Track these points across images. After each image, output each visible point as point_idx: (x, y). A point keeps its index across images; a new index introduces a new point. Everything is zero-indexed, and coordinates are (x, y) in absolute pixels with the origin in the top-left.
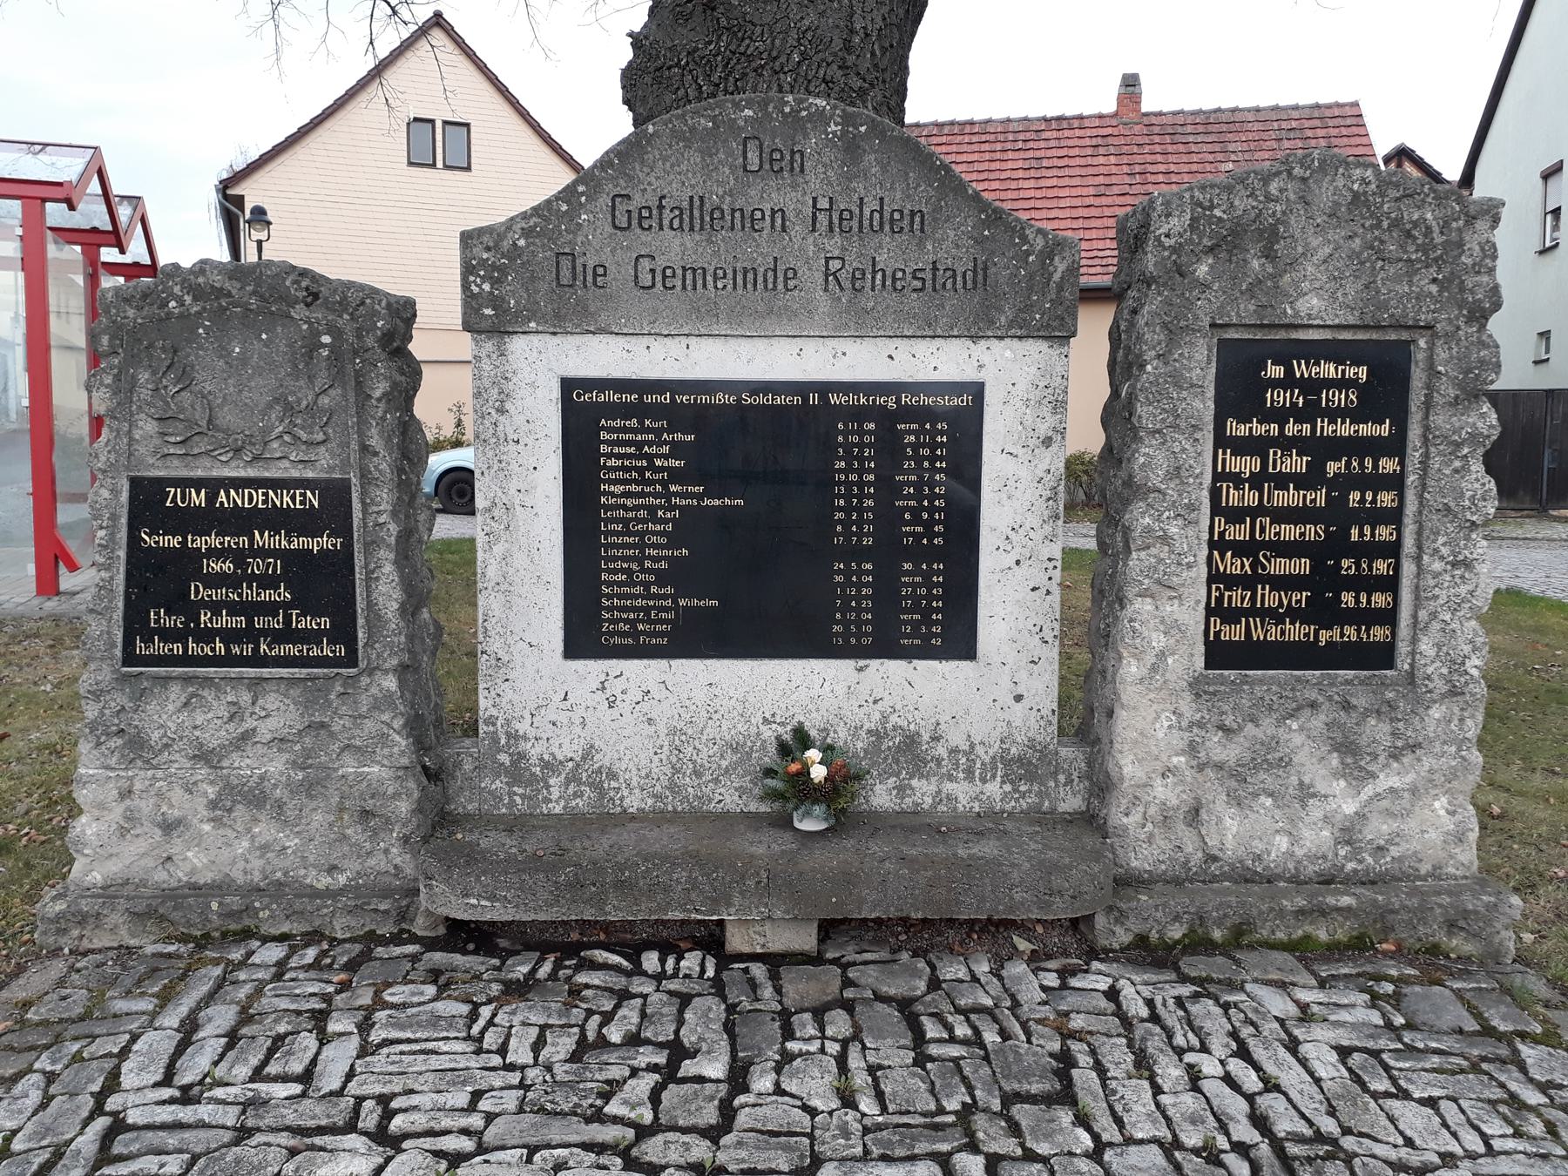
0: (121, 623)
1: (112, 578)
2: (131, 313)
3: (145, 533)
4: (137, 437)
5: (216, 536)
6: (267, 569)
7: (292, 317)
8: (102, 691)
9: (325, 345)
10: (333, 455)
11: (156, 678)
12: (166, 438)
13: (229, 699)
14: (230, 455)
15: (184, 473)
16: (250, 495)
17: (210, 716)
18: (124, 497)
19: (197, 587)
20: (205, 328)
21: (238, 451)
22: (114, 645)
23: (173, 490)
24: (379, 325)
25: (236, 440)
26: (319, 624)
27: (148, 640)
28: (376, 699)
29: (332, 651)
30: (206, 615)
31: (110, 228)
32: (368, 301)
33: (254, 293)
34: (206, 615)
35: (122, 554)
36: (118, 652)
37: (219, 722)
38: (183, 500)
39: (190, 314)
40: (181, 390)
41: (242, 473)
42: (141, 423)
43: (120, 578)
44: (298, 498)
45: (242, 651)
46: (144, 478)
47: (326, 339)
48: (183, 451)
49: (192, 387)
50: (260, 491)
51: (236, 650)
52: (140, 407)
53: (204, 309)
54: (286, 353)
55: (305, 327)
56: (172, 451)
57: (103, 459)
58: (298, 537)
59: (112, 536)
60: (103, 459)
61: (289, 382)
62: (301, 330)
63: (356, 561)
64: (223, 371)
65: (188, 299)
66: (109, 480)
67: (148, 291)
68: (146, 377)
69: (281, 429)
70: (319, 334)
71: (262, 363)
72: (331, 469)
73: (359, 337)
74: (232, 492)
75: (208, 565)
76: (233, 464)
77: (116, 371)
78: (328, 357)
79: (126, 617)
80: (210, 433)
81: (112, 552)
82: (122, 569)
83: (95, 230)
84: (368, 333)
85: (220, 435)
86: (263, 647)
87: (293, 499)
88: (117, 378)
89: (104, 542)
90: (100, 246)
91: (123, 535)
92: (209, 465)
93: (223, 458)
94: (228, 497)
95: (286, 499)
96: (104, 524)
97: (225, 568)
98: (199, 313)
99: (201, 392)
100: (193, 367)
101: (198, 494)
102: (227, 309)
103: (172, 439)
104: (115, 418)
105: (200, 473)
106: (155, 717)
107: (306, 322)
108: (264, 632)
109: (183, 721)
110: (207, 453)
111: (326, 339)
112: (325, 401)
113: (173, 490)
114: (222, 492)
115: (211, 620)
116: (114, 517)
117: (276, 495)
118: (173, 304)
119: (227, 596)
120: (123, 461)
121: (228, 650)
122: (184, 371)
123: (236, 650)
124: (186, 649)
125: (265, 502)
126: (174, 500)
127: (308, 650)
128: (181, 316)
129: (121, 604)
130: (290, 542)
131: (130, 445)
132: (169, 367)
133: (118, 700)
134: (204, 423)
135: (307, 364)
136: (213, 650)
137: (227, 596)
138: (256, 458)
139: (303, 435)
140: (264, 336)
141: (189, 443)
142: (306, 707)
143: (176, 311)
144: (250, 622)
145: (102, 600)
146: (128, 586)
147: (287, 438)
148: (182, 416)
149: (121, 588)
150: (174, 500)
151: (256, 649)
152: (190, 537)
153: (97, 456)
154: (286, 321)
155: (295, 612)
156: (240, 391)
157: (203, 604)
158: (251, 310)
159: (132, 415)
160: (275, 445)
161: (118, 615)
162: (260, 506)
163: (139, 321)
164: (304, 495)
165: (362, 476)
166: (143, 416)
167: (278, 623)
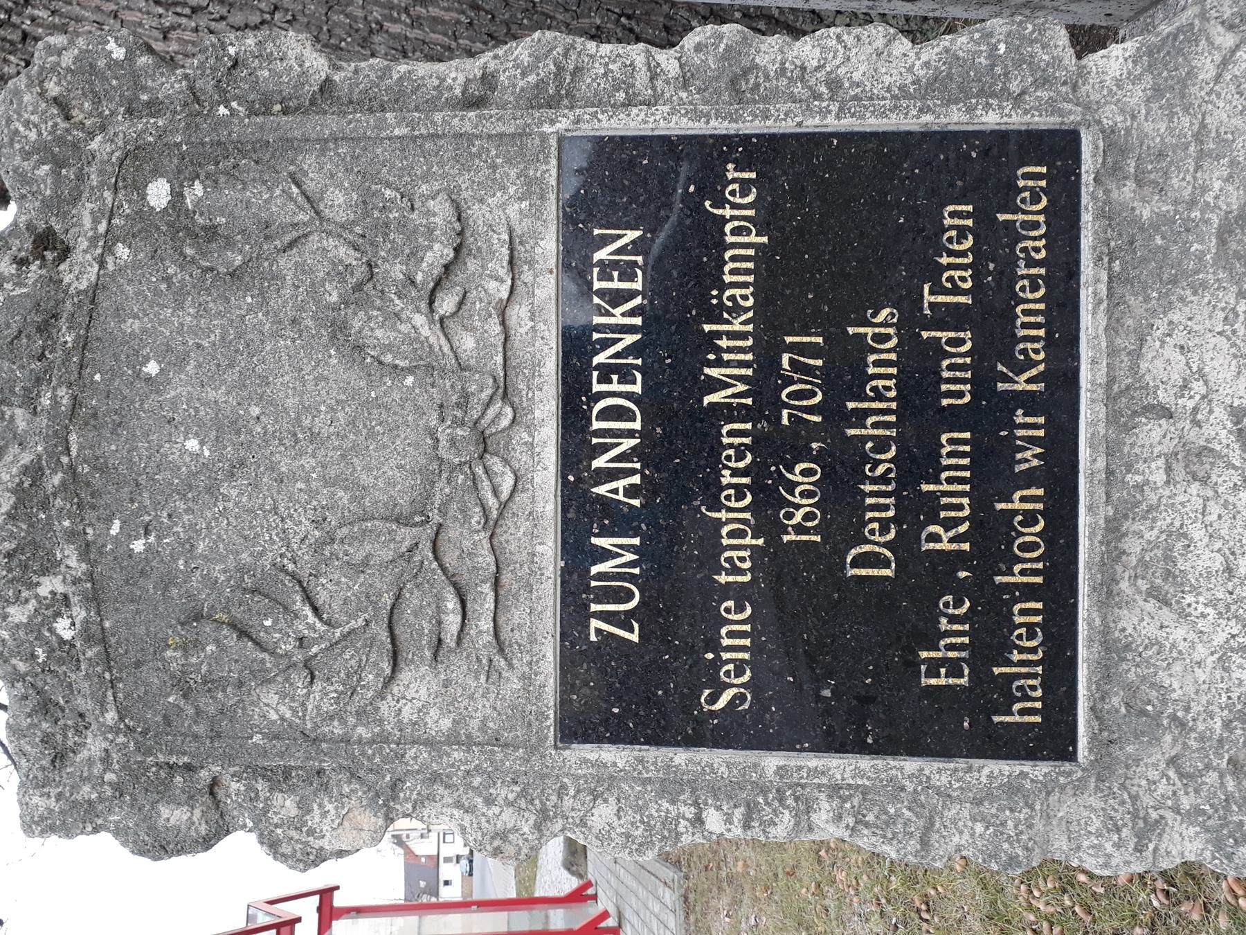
0: (961, 763)
1: (835, 790)
2: (94, 745)
3: (713, 699)
4: (446, 724)
5: (717, 507)
6: (808, 370)
7: (95, 287)
8: (1135, 816)
9: (177, 196)
10: (494, 184)
11: (1106, 674)
12: (449, 640)
13: (1159, 477)
14: (496, 464)
15: (548, 592)
16: (605, 414)
17: (1197, 533)
18: (615, 756)
19: (858, 562)
20: (129, 534)
21: (484, 443)
22: (1013, 788)
23: (595, 623)
24: (119, 53)
25: (453, 441)
26: (962, 233)
27: (1005, 694)
28: (1158, 92)
29: (1036, 199)
30: (935, 538)
31: (317, 897)
32: (53, 89)
33: (30, 402)
34: (935, 538)
35: (771, 762)
36: (1040, 770)
37: (1215, 509)
38: (623, 596)
39: (90, 576)
40: (309, 599)
41: (548, 433)
42: (408, 713)
43: (841, 767)
44: (616, 284)
45: (1033, 441)
46: (564, 703)
47: (158, 193)
48: (487, 588)
49: (304, 573)
50: (596, 387)
51: (1030, 458)
52: (361, 714)
53: (72, 536)
54: (202, 309)
55: (122, 251)
56: (486, 625)
57: (508, 818)
58: (723, 287)
59: (721, 792)
60: (508, 818)
61: (285, 299)
62: (135, 265)
63: (788, 126)
64: (255, 485)
65: (49, 585)
66: (568, 802)
67: (33, 700)
68: (273, 699)
69: (419, 320)
70: (143, 214)
71: (231, 376)
72: (532, 189)
73: (154, 107)
74: (600, 462)
75: (799, 529)
76: (521, 457)
77: (261, 785)
78: (212, 181)
79: (944, 752)
80: (436, 518)
81: (764, 791)
82: (813, 761)
83: (320, 909)
84: (144, 89)
85: (442, 489)
86: (1021, 384)
87: (616, 298)
88: (281, 779)
89: (738, 813)
90: (332, 907)
91: (719, 760)
92: (525, 526)
93: (507, 484)
94: (612, 475)
95: (618, 316)
96: (690, 812)
97: (806, 483)
98: (85, 551)
99: (318, 547)
100: (242, 569)
101: (606, 555)
102: (72, 469)
103: (452, 622)
104: (395, 786)
105: (548, 550)
106: (1201, 675)
107: (109, 249)
108: (983, 382)
109: (1212, 603)
110: (492, 526)
111: (158, 193)
112: (338, 201)
113: (595, 623)
114: (602, 490)
115: (949, 524)
116: (670, 786)
117: (605, 448)
118: (63, 628)
119: (883, 479)
120: (512, 761)
121: (1029, 478)
122: (254, 591)
123: (1030, 458)
124: (1029, 592)
125: (626, 378)
126: (623, 621)
127: (1031, 263)
128: (94, 599)
129: (911, 765)
130: (737, 310)
131: (469, 743)
132: (243, 634)
133: (1153, 774)
134: (406, 535)
135: (230, 243)
136: (1030, 519)
137: (883, 479)
138: (505, 392)
139: (439, 253)
140: (152, 368)
141: (464, 579)
142: (1174, 281)
143: (80, 613)
144: (954, 418)
145: (891, 821)
146: (861, 748)
147: (446, 304)
148: (387, 599)
149: (866, 763)
150: (623, 621)
151: (1029, 402)
152: (723, 579)
153: (503, 835)
154: (105, 303)
155: (928, 298)
156: (314, 437)
157: (905, 546)
158: (76, 403)
159: (385, 738)
160: (468, 343)
161: (938, 771)
162: (637, 388)
163: (111, 716)
164: (606, 373)
165: (553, 103)
166: (386, 708)
167: (960, 342)
